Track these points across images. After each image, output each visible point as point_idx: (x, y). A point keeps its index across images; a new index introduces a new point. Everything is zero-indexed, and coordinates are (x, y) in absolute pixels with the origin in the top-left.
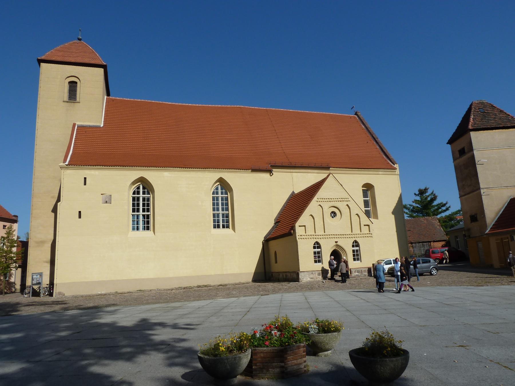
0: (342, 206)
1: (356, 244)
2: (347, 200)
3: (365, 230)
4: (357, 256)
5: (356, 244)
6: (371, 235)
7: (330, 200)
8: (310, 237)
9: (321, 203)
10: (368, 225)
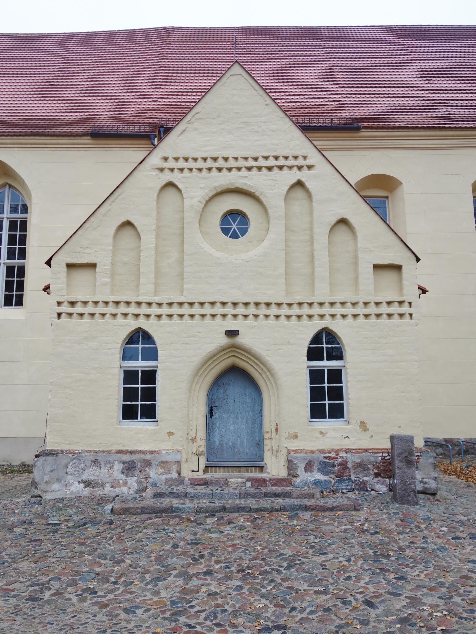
0: (273, 186)
1: (324, 345)
2: (300, 162)
3: (370, 287)
4: (327, 397)
5: (324, 345)
6: (405, 309)
7: (218, 164)
8: (111, 309)
9: (176, 177)
10: (399, 268)
